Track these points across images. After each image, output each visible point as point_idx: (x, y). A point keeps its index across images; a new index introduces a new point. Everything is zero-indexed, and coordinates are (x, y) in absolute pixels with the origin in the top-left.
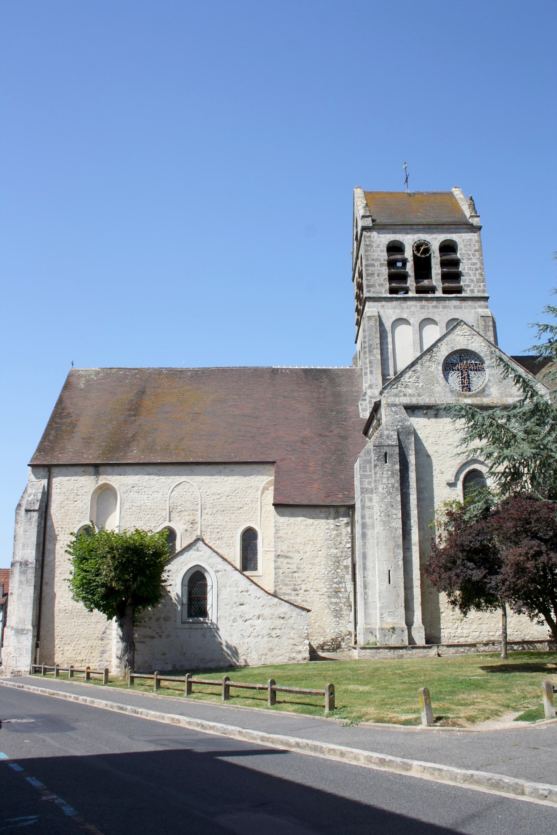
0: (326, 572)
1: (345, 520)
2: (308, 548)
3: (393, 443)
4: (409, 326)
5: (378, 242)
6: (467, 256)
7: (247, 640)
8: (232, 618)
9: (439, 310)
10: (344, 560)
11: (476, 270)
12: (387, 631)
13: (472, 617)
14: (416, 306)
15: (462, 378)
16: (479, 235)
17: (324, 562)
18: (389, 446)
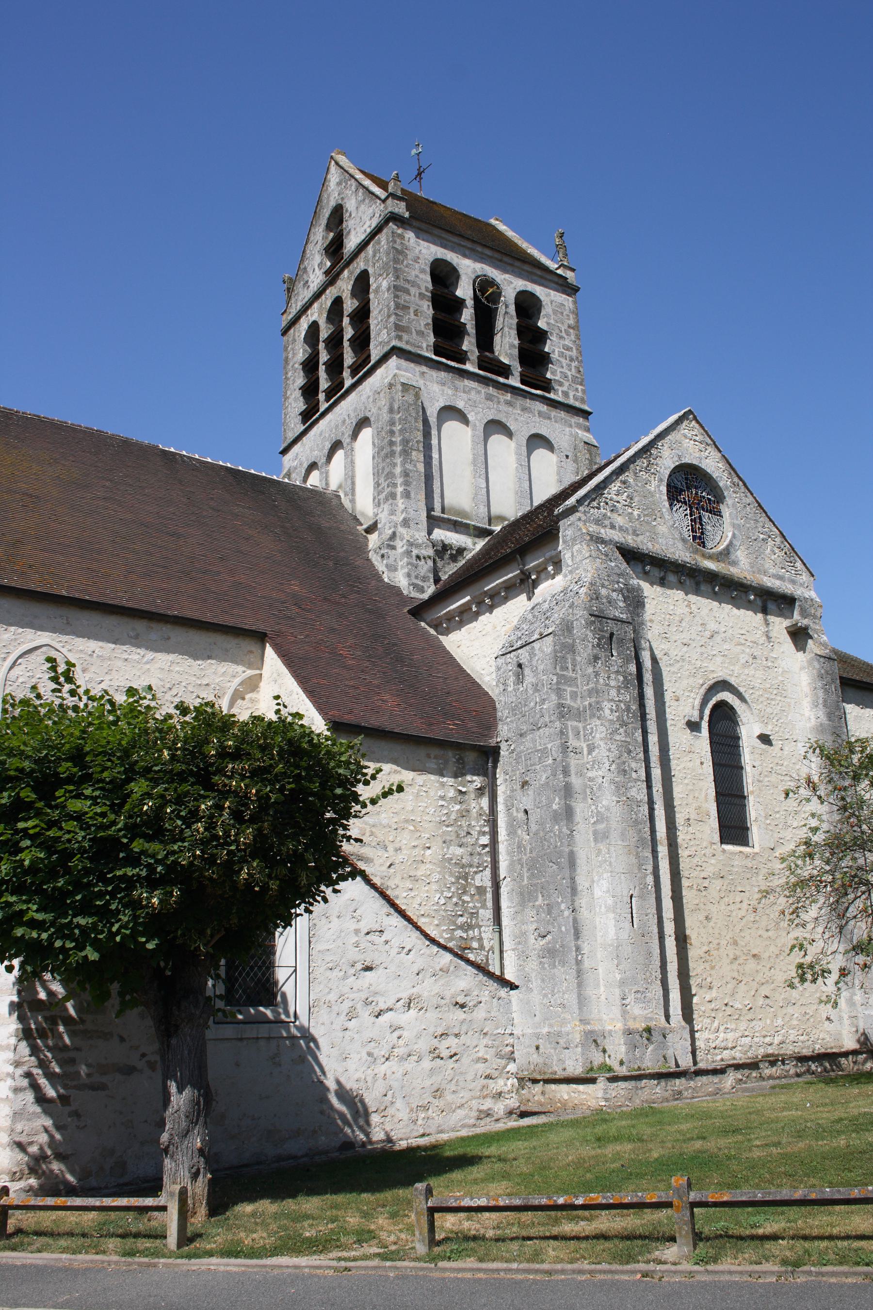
0: (442, 901)
1: (478, 781)
2: (405, 839)
3: (621, 616)
4: (464, 426)
5: (417, 251)
6: (557, 331)
7: (382, 1069)
8: (347, 1004)
9: (515, 411)
10: (476, 873)
11: (572, 360)
12: (638, 1037)
13: (740, 1006)
14: (479, 392)
15: (691, 520)
16: (575, 302)
17: (436, 876)
18: (616, 619)
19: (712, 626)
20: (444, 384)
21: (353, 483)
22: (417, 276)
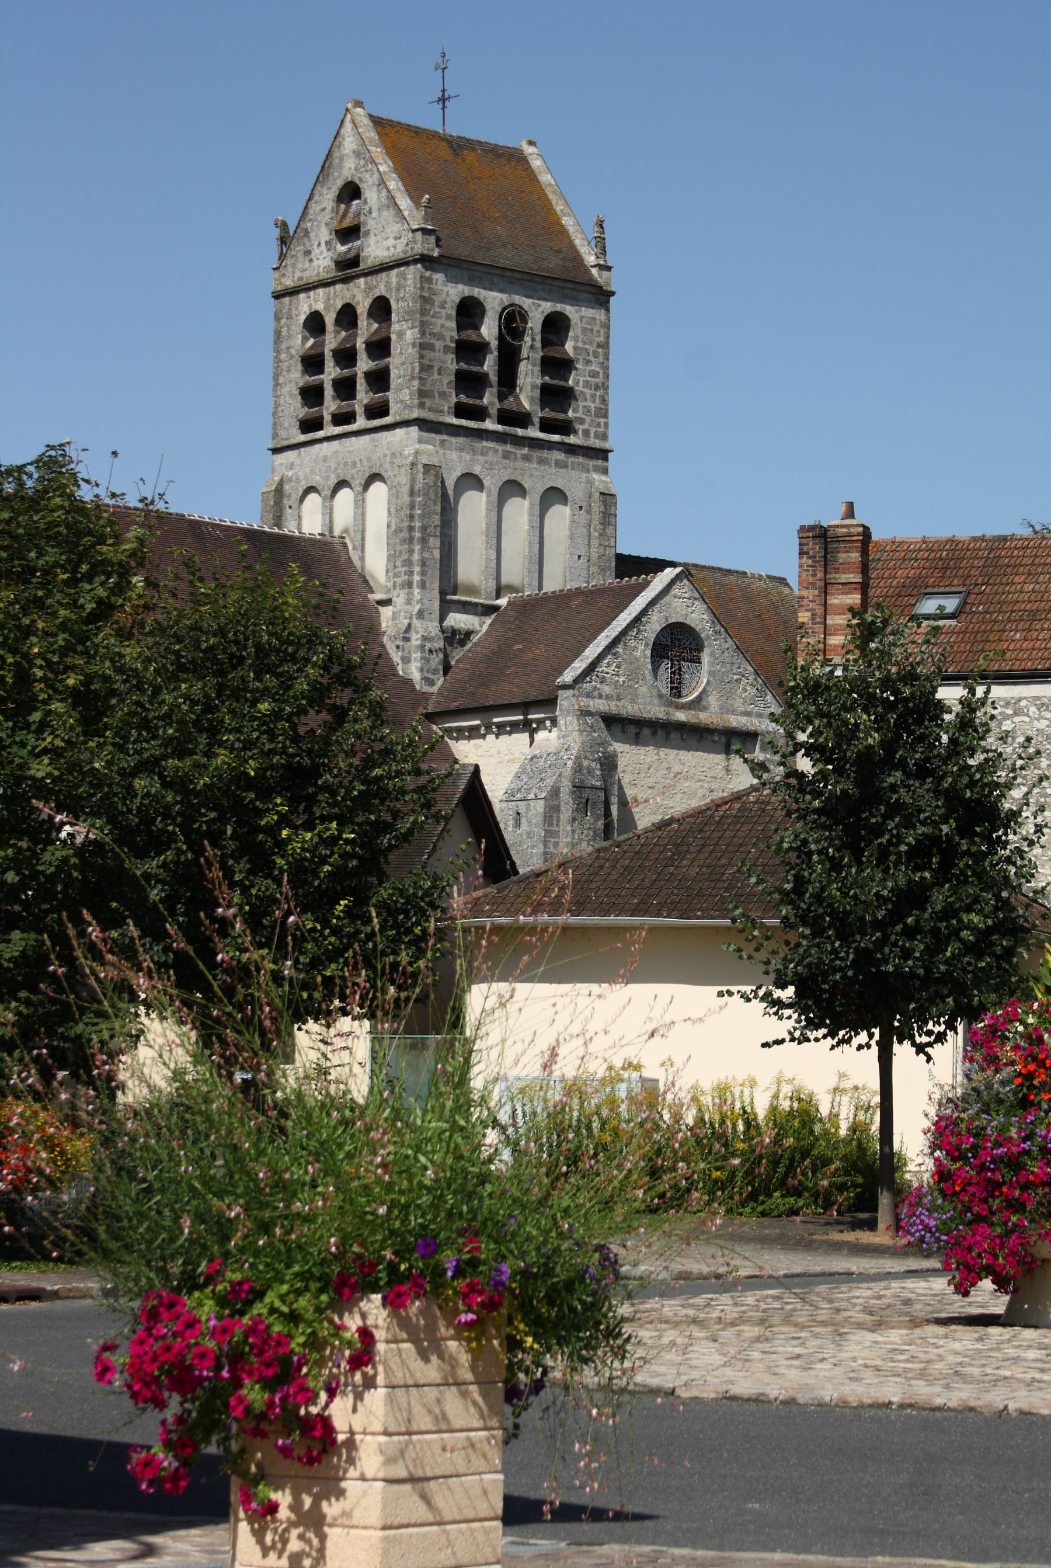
14: (496, 451)
18: (593, 787)
19: (677, 768)
20: (462, 450)
21: (363, 539)
22: (443, 326)
